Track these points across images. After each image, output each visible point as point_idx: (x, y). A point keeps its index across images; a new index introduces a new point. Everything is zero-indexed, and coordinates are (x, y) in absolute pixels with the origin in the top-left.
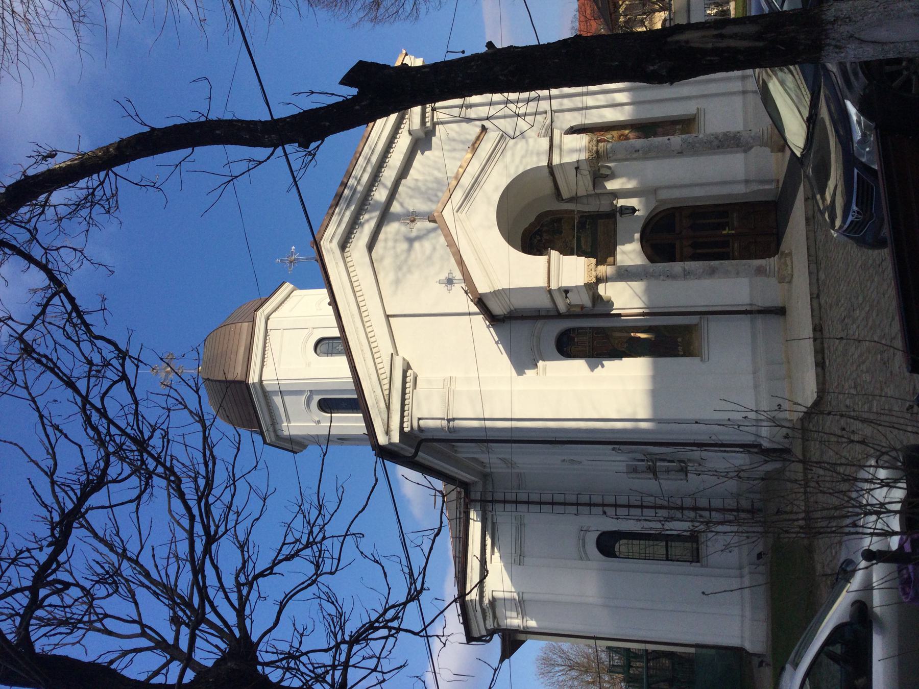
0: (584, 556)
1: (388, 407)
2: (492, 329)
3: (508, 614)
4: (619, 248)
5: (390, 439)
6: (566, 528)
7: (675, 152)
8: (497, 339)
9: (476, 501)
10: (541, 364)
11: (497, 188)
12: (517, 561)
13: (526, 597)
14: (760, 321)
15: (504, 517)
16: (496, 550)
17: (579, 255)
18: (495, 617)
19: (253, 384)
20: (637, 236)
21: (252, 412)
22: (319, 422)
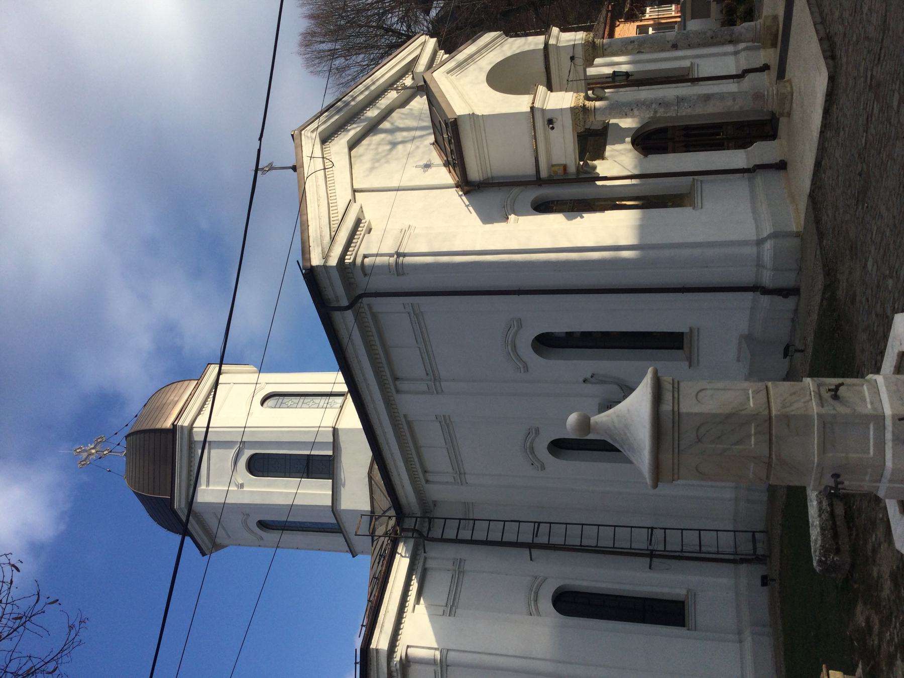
0: (533, 610)
1: (333, 239)
2: (464, 198)
4: (608, 148)
5: (326, 262)
6: (520, 568)
7: (670, 44)
8: (467, 203)
9: (408, 530)
10: (512, 217)
11: (491, 63)
12: (448, 609)
13: (452, 656)
14: (760, 179)
15: (440, 557)
16: (422, 601)
19: (182, 427)
20: (628, 139)
21: (169, 480)
22: (242, 486)
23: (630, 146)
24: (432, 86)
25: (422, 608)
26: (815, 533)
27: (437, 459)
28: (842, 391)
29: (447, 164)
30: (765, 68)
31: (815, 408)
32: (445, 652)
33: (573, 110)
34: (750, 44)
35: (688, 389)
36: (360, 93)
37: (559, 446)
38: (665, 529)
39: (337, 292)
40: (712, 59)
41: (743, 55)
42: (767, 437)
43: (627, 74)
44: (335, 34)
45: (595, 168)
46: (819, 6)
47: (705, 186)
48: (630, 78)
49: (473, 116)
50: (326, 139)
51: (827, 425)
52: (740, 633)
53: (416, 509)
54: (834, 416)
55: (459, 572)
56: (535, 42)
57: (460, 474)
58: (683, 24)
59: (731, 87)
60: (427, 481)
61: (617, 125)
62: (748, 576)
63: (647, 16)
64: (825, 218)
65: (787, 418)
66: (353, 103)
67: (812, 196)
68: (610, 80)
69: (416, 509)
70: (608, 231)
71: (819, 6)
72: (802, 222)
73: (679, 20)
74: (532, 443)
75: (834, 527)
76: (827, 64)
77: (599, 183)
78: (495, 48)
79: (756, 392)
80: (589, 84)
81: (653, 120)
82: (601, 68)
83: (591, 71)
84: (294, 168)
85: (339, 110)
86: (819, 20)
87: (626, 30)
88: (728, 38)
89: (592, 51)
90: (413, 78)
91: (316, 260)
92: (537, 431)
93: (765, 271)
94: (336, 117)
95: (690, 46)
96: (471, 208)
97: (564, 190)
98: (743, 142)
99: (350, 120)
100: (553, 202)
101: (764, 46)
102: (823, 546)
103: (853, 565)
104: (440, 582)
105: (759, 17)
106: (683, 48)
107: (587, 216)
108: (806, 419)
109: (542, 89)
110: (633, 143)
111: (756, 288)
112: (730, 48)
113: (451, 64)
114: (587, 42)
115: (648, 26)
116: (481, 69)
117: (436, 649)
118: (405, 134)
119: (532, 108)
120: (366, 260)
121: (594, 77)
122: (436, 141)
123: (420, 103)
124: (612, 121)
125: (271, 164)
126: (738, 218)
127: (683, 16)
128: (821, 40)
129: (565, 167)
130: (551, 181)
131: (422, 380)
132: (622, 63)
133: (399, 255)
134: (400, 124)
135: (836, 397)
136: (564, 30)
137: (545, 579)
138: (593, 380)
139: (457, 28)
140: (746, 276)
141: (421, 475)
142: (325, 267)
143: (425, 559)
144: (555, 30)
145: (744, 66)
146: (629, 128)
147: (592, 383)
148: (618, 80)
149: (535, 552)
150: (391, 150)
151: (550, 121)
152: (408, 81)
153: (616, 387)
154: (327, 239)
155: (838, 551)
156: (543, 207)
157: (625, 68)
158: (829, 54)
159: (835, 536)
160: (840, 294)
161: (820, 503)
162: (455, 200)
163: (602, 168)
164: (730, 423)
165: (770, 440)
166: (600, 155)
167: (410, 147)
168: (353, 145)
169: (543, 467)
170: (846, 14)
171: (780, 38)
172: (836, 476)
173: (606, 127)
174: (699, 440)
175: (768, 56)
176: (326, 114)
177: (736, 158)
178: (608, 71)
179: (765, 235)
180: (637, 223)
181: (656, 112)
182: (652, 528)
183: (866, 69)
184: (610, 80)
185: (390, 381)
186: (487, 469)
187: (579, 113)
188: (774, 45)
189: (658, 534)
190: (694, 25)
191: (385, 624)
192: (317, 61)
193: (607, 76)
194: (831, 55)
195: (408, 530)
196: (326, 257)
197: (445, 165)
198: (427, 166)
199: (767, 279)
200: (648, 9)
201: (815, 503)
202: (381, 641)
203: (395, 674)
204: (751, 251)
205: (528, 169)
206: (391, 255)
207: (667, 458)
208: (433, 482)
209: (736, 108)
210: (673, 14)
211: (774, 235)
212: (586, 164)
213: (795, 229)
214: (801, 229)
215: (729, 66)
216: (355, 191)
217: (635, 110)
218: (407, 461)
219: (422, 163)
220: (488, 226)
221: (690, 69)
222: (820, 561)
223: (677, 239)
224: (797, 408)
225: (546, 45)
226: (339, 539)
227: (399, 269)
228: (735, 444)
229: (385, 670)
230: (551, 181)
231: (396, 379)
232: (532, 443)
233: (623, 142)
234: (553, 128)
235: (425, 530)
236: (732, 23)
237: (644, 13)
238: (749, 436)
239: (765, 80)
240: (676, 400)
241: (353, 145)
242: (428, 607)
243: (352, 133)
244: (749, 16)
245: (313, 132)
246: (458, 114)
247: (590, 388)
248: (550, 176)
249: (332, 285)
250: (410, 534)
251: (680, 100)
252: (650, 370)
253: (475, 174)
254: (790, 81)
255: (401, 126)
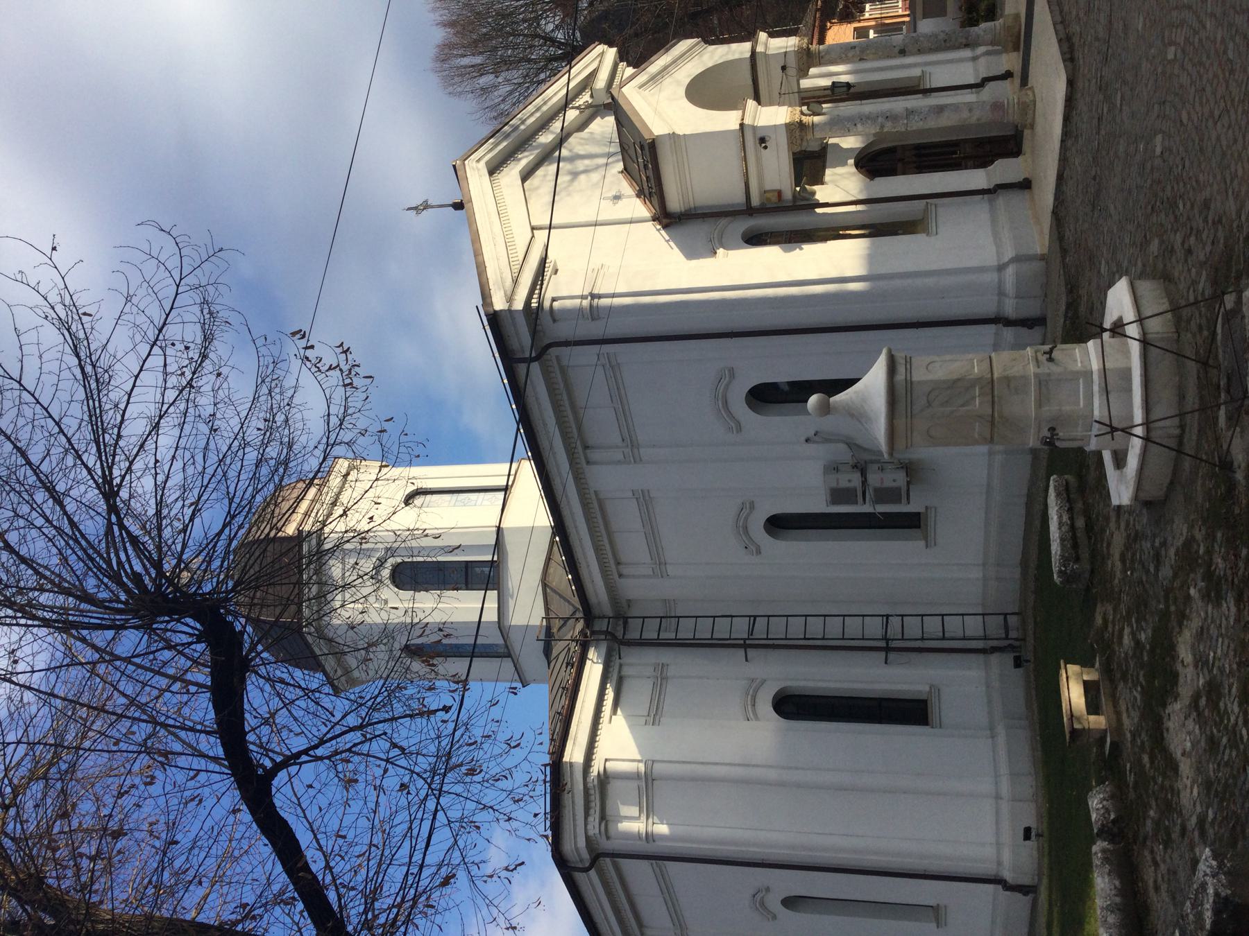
1: (515, 282)
2: (663, 232)
3: (626, 810)
4: (828, 172)
7: (897, 50)
10: (721, 251)
13: (658, 768)
14: (1001, 200)
15: (638, 663)
16: (619, 711)
17: (779, 104)
18: (603, 817)
20: (851, 161)
23: (854, 169)
24: (621, 101)
25: (620, 719)
26: (1055, 547)
27: (633, 547)
28: (1055, 354)
29: (640, 194)
30: (1008, 75)
31: (1032, 368)
32: (649, 763)
33: (789, 127)
34: (990, 48)
35: (919, 362)
36: (529, 115)
37: (779, 524)
38: (902, 616)
39: (522, 338)
40: (949, 66)
41: (982, 60)
42: (990, 397)
43: (848, 85)
44: (473, 47)
45: (814, 193)
46: (1060, 4)
47: (940, 210)
48: (852, 90)
49: (673, 136)
50: (494, 169)
51: (1043, 383)
52: (992, 728)
53: (607, 610)
54: (1049, 375)
55: (661, 679)
56: (740, 50)
57: (660, 564)
58: (913, 25)
59: (969, 97)
60: (620, 576)
61: (837, 145)
62: (1000, 664)
63: (867, 15)
64: (1067, 233)
65: (1007, 380)
66: (522, 127)
67: (1055, 213)
68: (829, 92)
69: (607, 610)
70: (836, 262)
71: (1060, 4)
72: (1047, 243)
73: (907, 19)
74: (746, 519)
75: (1074, 537)
76: (1066, 67)
77: (819, 210)
78: (692, 58)
79: (980, 361)
80: (803, 99)
81: (879, 137)
82: (817, 79)
83: (806, 83)
84: (459, 206)
85: (507, 136)
86: (1059, 19)
87: (841, 34)
88: (964, 41)
89: (807, 59)
90: (592, 96)
91: (499, 304)
92: (752, 506)
93: (1007, 301)
94: (505, 144)
95: (920, 52)
96: (672, 243)
97: (780, 219)
98: (983, 161)
99: (526, 149)
100: (766, 234)
101: (1005, 51)
102: (1062, 556)
103: (1092, 571)
104: (640, 691)
105: (1002, 16)
106: (912, 54)
107: (807, 248)
108: (1025, 378)
109: (751, 103)
110: (857, 165)
111: (998, 320)
112: (967, 53)
113: (642, 78)
114: (800, 48)
115: (867, 29)
116: (678, 83)
117: (639, 761)
118: (587, 162)
119: (742, 125)
120: (556, 304)
121: (807, 90)
122: (625, 169)
123: (605, 125)
124: (831, 141)
125: (426, 201)
126: (977, 243)
127: (913, 14)
128: (1060, 41)
129: (779, 193)
130: (764, 210)
131: (617, 447)
132: (842, 73)
133: (593, 296)
134: (581, 150)
135: (1051, 360)
136: (772, 35)
137: (763, 682)
138: (816, 438)
139: (636, 35)
140: (988, 307)
141: (613, 567)
142: (510, 311)
143: (621, 665)
144: (763, 36)
145: (984, 74)
146: (851, 150)
147: (815, 442)
148: (839, 93)
149: (751, 652)
150: (572, 180)
151: (762, 140)
152: (585, 98)
153: (842, 446)
154: (509, 282)
155: (1077, 559)
156: (755, 239)
157: (844, 79)
158: (1068, 56)
159: (1075, 546)
160: (1082, 309)
161: (1060, 517)
162: (653, 235)
163: (822, 193)
164: (957, 387)
165: (993, 402)
166: (819, 180)
167: (595, 176)
168: (526, 176)
169: (759, 552)
170: (1082, 15)
171: (1021, 41)
172: (1052, 429)
173: (824, 148)
174: (929, 404)
175: (1009, 61)
176: (491, 141)
177: (976, 178)
178: (827, 82)
179: (1006, 260)
180: (866, 252)
181: (882, 127)
182: (888, 616)
183: (1097, 70)
184: (829, 92)
185: (580, 450)
186: (692, 551)
187: (796, 130)
188: (1016, 49)
189: (895, 622)
190: (927, 26)
191: (579, 735)
192: (456, 79)
193: (825, 89)
194: (1069, 58)
195: (600, 632)
196: (510, 300)
197: (638, 196)
198: (617, 198)
199: (1010, 308)
200: (868, 7)
201: (1055, 517)
202: (574, 753)
203: (592, 792)
204: (993, 277)
205: (738, 197)
206: (583, 297)
207: (901, 423)
208: (628, 576)
209: (973, 120)
210: (900, 12)
211: (1017, 259)
212: (803, 189)
213: (1039, 252)
214: (1046, 251)
215: (968, 74)
216: (533, 229)
217: (859, 125)
218: (598, 550)
219: (611, 194)
220: (694, 262)
221: (921, 78)
222: (1060, 572)
223: (910, 267)
224: (1016, 370)
225: (753, 53)
226: (507, 664)
227: (594, 313)
228: (963, 406)
229: (581, 787)
230: (764, 210)
231: (586, 447)
232: (746, 519)
233: (844, 164)
234: (766, 148)
235: (620, 635)
236: (973, 22)
237: (862, 11)
238: (974, 398)
239: (1006, 91)
240: (909, 370)
241: (526, 176)
242: (628, 717)
243: (524, 162)
244: (991, 14)
245: (478, 161)
246: (656, 133)
247: (812, 449)
248: (762, 204)
249: (517, 334)
250: (603, 637)
251: (910, 113)
252: (884, 351)
253: (675, 203)
254: (1032, 88)
255: (582, 153)
